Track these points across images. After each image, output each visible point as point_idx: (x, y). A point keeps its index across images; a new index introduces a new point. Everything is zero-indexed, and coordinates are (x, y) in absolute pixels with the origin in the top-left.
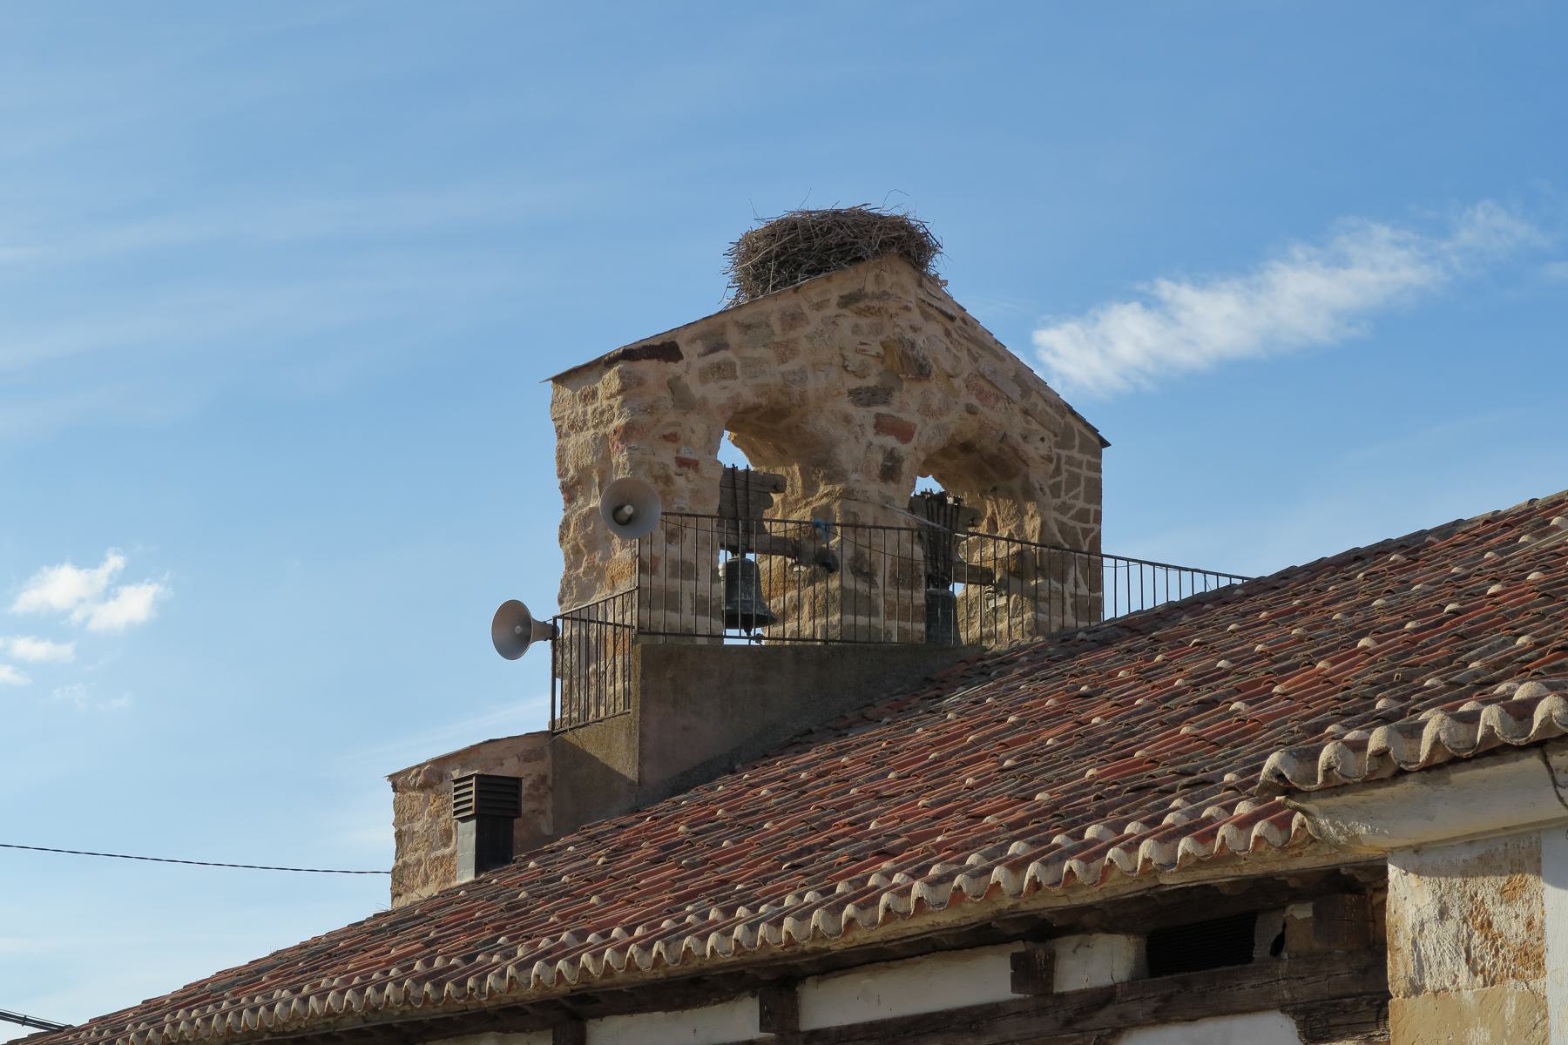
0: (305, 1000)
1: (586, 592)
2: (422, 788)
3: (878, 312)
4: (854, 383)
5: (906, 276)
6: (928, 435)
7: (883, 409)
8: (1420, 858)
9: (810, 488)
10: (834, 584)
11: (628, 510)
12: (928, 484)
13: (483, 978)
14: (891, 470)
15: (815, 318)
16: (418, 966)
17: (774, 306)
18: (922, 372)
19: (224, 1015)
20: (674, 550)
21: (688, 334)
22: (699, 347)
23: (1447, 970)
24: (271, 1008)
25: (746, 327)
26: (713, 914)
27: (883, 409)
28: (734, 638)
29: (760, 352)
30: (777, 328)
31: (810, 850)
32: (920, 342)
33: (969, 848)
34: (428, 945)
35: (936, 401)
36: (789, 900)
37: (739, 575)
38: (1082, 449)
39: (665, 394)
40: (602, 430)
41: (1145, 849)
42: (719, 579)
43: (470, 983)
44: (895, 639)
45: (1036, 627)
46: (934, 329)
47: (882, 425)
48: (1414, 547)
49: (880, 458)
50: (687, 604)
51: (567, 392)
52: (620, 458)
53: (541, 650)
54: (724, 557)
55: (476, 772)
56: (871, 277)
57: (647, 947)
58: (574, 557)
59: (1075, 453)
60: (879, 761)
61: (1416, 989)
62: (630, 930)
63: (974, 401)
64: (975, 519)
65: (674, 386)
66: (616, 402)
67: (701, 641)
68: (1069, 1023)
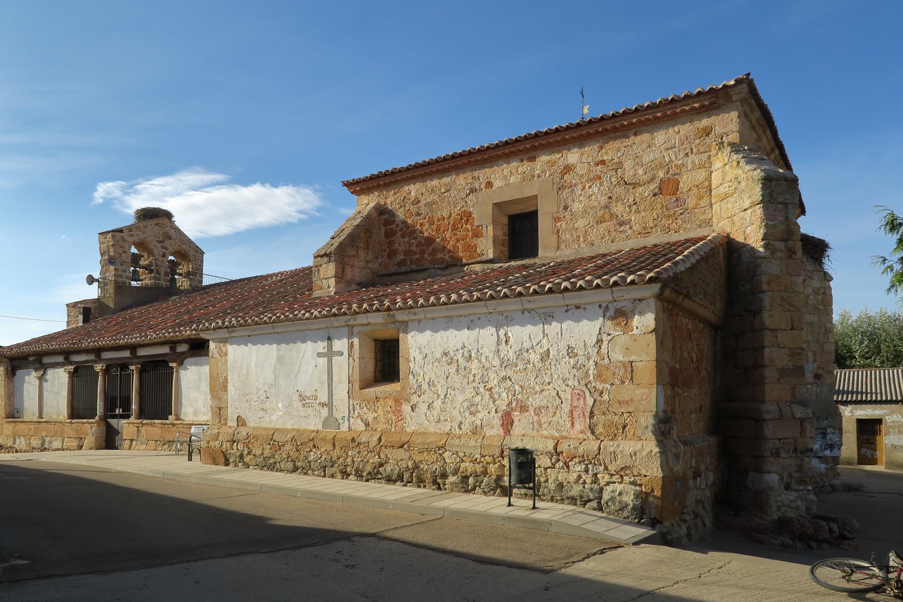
0: (49, 346)
1: (105, 273)
2: (72, 307)
3: (162, 227)
4: (157, 239)
5: (168, 221)
6: (171, 249)
7: (163, 244)
8: (214, 340)
9: (149, 257)
10: (152, 275)
11: (112, 261)
12: (171, 258)
13: (82, 345)
14: (164, 255)
15: (150, 227)
16: (70, 341)
17: (142, 224)
18: (170, 238)
19: (33, 348)
20: (122, 267)
21: (125, 228)
22: (127, 231)
23: (216, 355)
24: (42, 347)
25: (136, 228)
26: (122, 337)
27: (163, 244)
28: (134, 283)
29: (139, 232)
30: (142, 228)
31: (140, 326)
32: (170, 233)
33: (163, 329)
34: (72, 338)
35: (173, 243)
36: (134, 335)
37: (135, 272)
38: (200, 254)
39: (121, 239)
40: (108, 244)
41: (188, 332)
42: (130, 273)
43: (80, 345)
44: (164, 286)
45: (190, 285)
46: (173, 231)
47: (162, 247)
48: (256, 278)
49: (162, 253)
50: (125, 277)
51: (101, 236)
52: (111, 250)
53: (96, 284)
54: (132, 268)
55: (83, 306)
56: (161, 220)
57: (110, 342)
58: (103, 267)
59: (199, 255)
60: (156, 310)
61: (212, 357)
62: (108, 338)
63: (180, 244)
64: (180, 264)
65: (122, 238)
66: (111, 239)
67: (127, 285)
68: (178, 357)
